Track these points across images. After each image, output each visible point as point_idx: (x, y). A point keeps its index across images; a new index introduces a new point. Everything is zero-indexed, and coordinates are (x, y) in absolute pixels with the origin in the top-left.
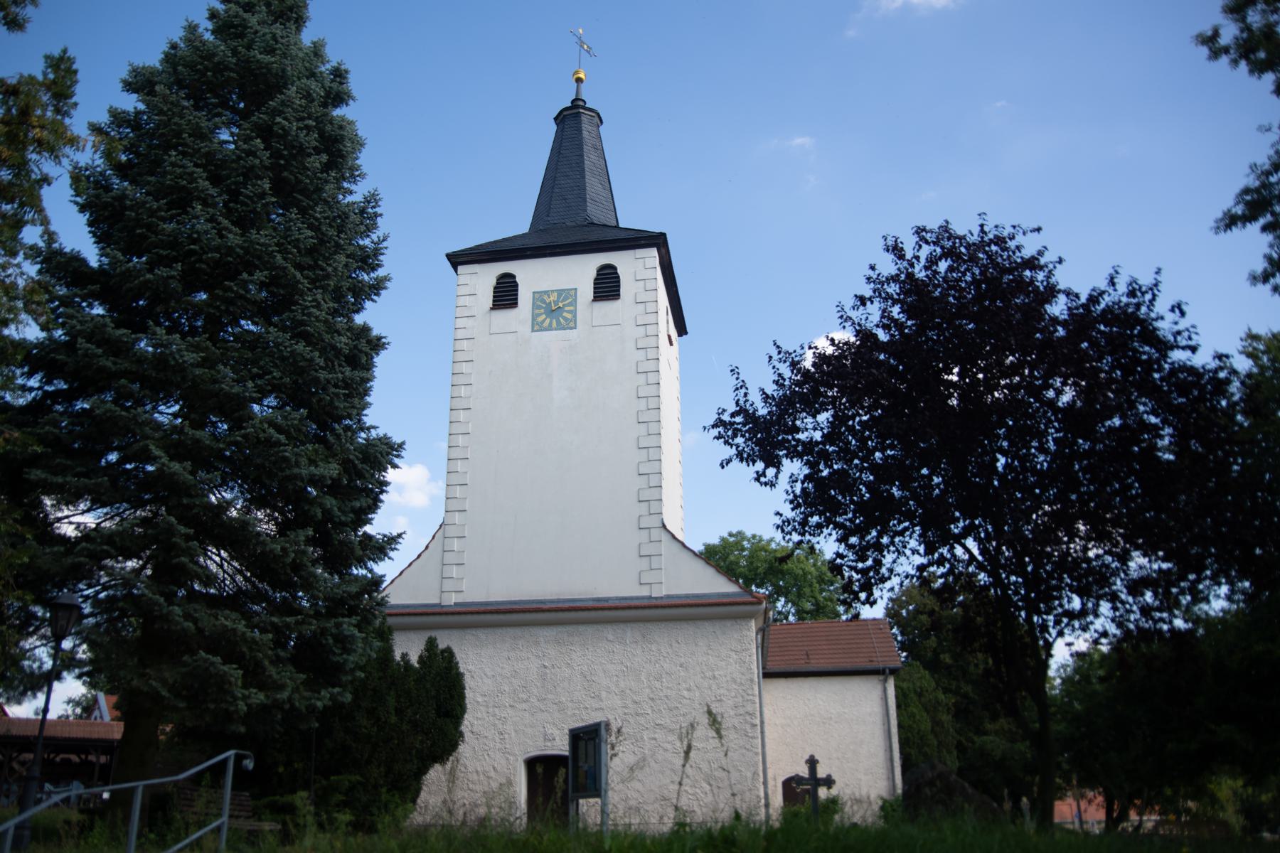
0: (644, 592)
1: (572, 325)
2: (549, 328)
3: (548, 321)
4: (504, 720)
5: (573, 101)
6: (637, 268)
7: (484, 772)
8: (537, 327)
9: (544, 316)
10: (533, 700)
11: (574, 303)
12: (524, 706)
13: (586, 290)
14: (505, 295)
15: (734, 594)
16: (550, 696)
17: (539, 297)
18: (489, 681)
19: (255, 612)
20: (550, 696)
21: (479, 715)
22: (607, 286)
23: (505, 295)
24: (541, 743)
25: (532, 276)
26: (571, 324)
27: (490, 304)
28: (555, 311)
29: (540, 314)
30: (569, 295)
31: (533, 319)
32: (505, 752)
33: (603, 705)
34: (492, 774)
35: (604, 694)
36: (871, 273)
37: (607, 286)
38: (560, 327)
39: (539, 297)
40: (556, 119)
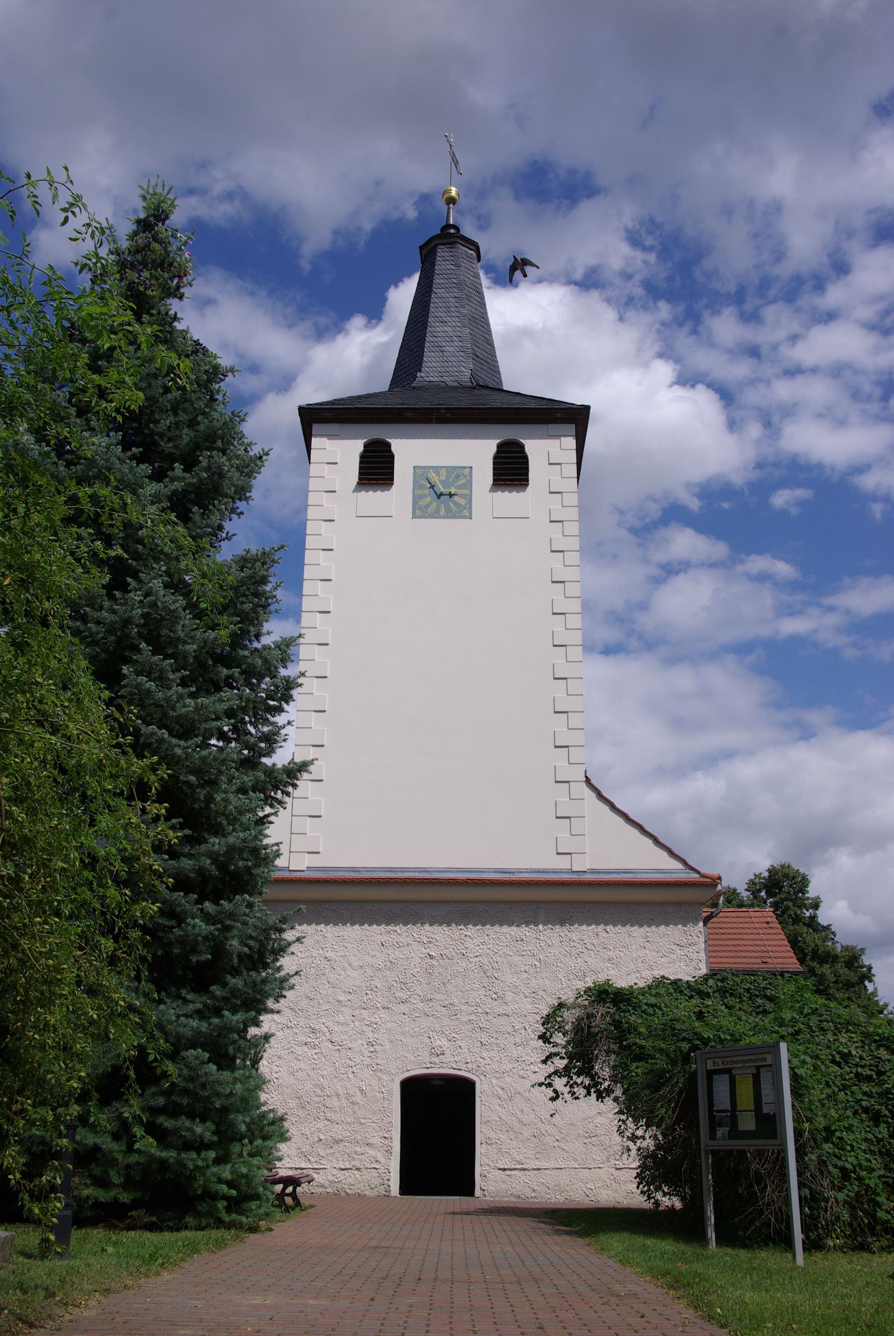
0: (563, 863)
1: (418, 513)
2: (435, 515)
3: (434, 505)
4: (374, 1026)
5: (443, 229)
6: (545, 451)
7: (348, 1096)
8: (419, 511)
9: (429, 499)
10: (415, 1000)
11: (469, 485)
12: (403, 1008)
13: (484, 473)
14: (376, 469)
15: (677, 871)
16: (438, 996)
17: (420, 473)
18: (355, 974)
19: (250, 733)
20: (438, 996)
21: (341, 1019)
22: (511, 470)
23: (376, 469)
24: (426, 1057)
25: (411, 452)
26: (464, 511)
27: (356, 479)
28: (442, 496)
29: (424, 496)
30: (462, 474)
31: (415, 502)
32: (376, 1069)
33: (509, 1009)
34: (359, 1098)
35: (509, 996)
36: (239, 511)
37: (511, 470)
38: (450, 515)
39: (420, 473)
40: (421, 248)
